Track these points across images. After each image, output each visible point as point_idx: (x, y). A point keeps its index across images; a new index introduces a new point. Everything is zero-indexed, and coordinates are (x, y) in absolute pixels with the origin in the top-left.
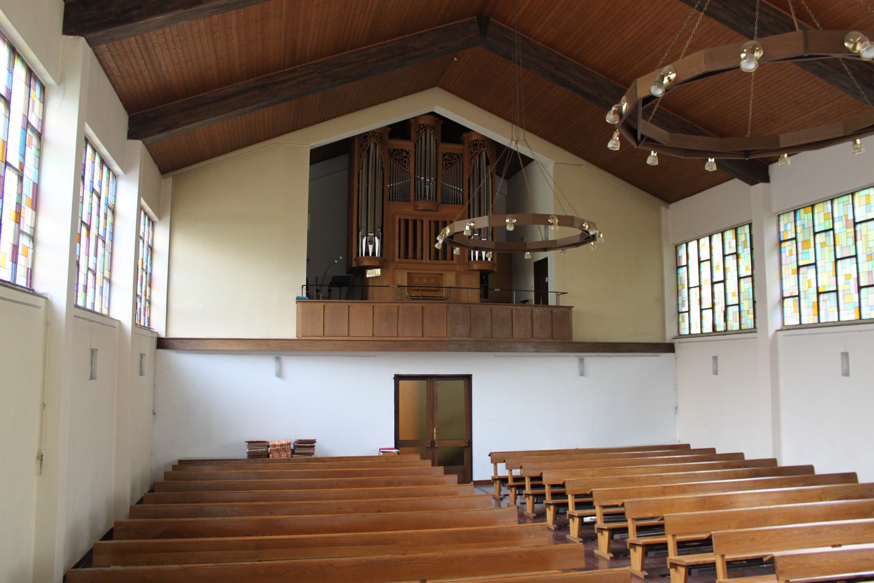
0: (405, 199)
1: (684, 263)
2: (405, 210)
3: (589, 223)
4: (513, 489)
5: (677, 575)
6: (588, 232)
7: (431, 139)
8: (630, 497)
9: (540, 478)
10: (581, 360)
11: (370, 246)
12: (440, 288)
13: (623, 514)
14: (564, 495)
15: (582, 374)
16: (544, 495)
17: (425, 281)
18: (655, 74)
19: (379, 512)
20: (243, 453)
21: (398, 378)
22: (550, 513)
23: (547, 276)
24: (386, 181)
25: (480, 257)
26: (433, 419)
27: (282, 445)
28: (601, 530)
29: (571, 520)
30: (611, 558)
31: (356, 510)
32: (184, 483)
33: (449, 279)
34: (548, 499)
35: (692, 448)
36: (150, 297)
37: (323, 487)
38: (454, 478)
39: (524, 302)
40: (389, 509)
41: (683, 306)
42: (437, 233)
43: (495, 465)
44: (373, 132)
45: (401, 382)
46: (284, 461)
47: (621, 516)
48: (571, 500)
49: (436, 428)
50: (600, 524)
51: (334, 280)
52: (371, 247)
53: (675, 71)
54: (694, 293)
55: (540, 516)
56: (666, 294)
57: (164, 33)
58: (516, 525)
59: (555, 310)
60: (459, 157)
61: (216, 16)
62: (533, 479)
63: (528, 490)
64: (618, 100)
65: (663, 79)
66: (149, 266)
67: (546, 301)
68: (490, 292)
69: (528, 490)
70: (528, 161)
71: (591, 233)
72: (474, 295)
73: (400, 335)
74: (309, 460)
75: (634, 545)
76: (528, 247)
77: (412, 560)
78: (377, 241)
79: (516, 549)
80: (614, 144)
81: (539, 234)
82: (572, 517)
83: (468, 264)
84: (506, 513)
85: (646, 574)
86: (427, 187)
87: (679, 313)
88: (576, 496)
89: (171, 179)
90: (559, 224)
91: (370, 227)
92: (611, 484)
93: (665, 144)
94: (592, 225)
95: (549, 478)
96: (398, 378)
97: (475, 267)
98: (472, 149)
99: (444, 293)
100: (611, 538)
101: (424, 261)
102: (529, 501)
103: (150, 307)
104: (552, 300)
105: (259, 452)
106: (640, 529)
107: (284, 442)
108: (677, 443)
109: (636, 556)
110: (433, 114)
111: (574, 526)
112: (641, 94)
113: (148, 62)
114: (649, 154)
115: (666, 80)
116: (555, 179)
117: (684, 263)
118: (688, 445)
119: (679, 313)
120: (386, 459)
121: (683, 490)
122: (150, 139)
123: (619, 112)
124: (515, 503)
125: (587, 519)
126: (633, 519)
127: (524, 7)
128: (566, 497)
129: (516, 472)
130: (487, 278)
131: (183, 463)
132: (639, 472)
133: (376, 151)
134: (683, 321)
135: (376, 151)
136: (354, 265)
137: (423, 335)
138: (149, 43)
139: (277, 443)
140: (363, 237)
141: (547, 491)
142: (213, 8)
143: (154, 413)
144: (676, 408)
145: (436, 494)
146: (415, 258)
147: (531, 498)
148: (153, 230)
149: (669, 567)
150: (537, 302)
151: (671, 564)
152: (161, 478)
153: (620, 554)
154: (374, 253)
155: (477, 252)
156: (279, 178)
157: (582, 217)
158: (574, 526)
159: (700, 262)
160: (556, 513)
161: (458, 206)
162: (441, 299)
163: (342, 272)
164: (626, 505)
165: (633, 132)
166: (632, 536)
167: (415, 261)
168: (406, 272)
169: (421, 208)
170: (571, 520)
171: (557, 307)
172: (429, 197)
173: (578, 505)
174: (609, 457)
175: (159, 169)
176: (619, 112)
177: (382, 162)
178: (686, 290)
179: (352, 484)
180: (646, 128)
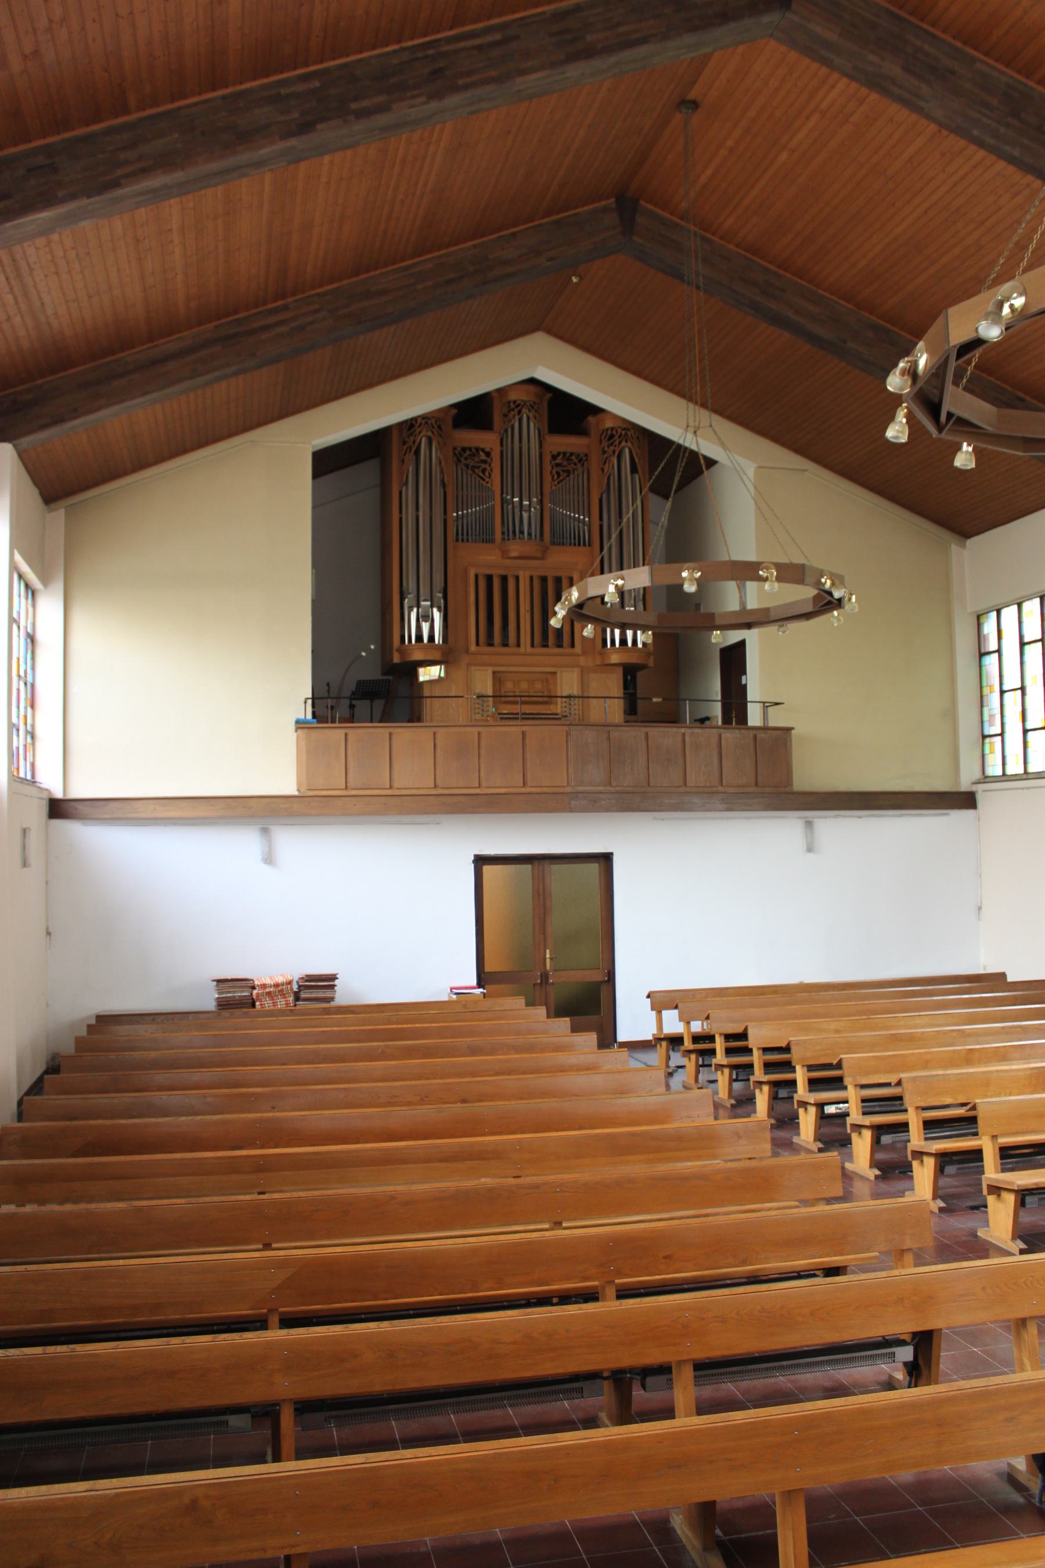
0: (488, 539)
1: (993, 646)
2: (486, 559)
3: (833, 577)
4: (693, 1057)
5: (1000, 1205)
6: (830, 594)
7: (530, 429)
8: (911, 1069)
9: (743, 1036)
10: (809, 824)
11: (425, 624)
12: (551, 698)
13: (900, 1098)
14: (788, 1066)
15: (810, 849)
16: (750, 1066)
17: (524, 686)
18: (985, 299)
19: (464, 1101)
20: (208, 1001)
21: (481, 861)
22: (762, 1099)
23: (745, 673)
24: (449, 507)
25: (623, 641)
26: (544, 933)
27: (277, 985)
28: (858, 1128)
29: (801, 1111)
30: (877, 1177)
31: (424, 1099)
32: (112, 1056)
33: (568, 683)
34: (758, 1073)
35: (1009, 979)
36: (33, 726)
37: (357, 1059)
38: (592, 1038)
39: (703, 720)
40: (481, 1098)
41: (991, 724)
42: (558, 599)
43: (659, 1013)
44: (424, 417)
45: (487, 869)
46: (282, 1013)
47: (895, 1102)
48: (801, 1076)
49: (551, 950)
50: (856, 1117)
51: (362, 688)
52: (425, 627)
53: (1023, 293)
54: (1013, 700)
55: (744, 1103)
56: (957, 702)
57: (49, 242)
58: (711, 1121)
59: (761, 735)
60: (582, 459)
61: (143, 210)
62: (728, 1037)
63: (720, 1058)
64: (908, 350)
65: (1000, 305)
66: (29, 671)
67: (743, 719)
68: (640, 703)
69: (720, 1058)
70: (711, 463)
71: (837, 595)
72: (615, 710)
73: (484, 784)
74: (327, 1011)
75: (919, 1155)
76: (718, 621)
77: (537, 1186)
78: (437, 615)
79: (717, 1163)
80: (897, 431)
81: (730, 597)
82: (804, 1104)
83: (601, 654)
84: (693, 1100)
85: (942, 1205)
86: (525, 515)
87: (984, 737)
88: (810, 1068)
89: (62, 512)
90: (779, 579)
91: (424, 591)
92: (872, 1046)
93: (990, 429)
94: (838, 580)
95: (759, 1036)
96: (481, 861)
97: (615, 659)
98: (605, 444)
99: (559, 707)
100: (876, 1142)
101: (522, 649)
102: (723, 1078)
103: (33, 744)
104: (754, 717)
105: (237, 998)
106: (929, 1125)
107: (280, 979)
108: (982, 972)
109: (924, 1174)
110: (533, 381)
111: (807, 1121)
112: (958, 336)
113: (20, 299)
114: (960, 448)
115: (1006, 310)
116: (760, 499)
117: (993, 646)
118: (1003, 975)
119: (984, 737)
120: (465, 1006)
121: (1002, 1056)
122: (26, 441)
123: (912, 373)
124: (697, 1080)
125: (831, 1109)
126: (917, 1108)
127: (704, 178)
128: (793, 1070)
129: (696, 1027)
130: (634, 678)
131: (105, 1021)
132: (921, 1023)
133: (431, 454)
134: (992, 752)
135: (431, 453)
136: (396, 659)
137: (525, 784)
138: (23, 264)
139: (268, 981)
140: (411, 609)
141: (757, 1059)
142: (141, 194)
143: (49, 934)
144: (980, 908)
145: (562, 1069)
146: (505, 644)
147: (726, 1071)
148: (34, 606)
149: (985, 1191)
150: (727, 720)
151: (989, 1186)
152: (68, 1048)
153: (894, 1169)
154: (431, 638)
155: (617, 632)
156: (255, 508)
157: (821, 566)
158: (807, 1121)
159: (1022, 645)
160: (774, 1098)
161: (582, 549)
162: (554, 717)
163: (373, 673)
164: (904, 1084)
165: (933, 408)
166: (916, 1139)
167: (505, 650)
168: (490, 670)
169: (514, 554)
170: (801, 1111)
171: (765, 728)
172: (530, 534)
173: (814, 1084)
174: (866, 997)
175: (42, 494)
176: (912, 373)
177: (442, 472)
178: (995, 697)
179: (409, 1053)
180: (957, 401)
